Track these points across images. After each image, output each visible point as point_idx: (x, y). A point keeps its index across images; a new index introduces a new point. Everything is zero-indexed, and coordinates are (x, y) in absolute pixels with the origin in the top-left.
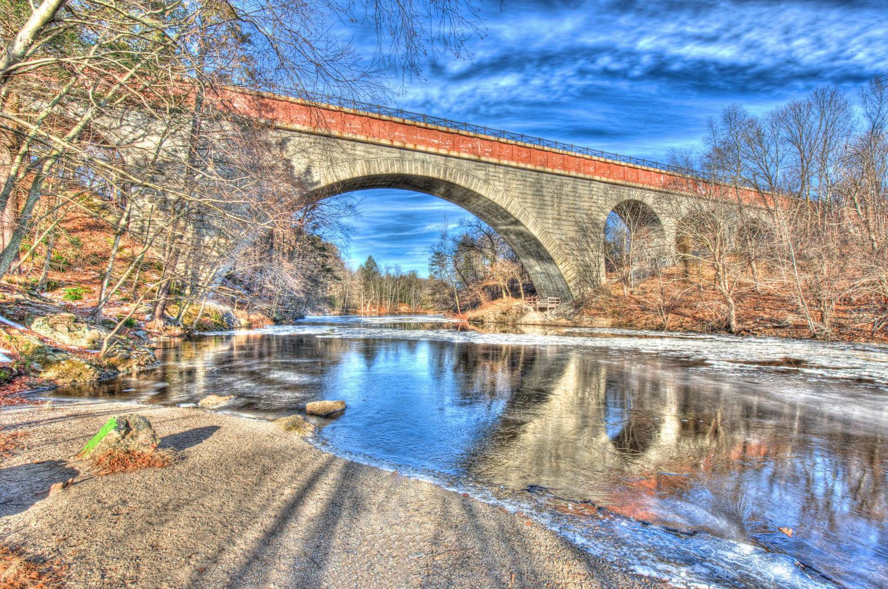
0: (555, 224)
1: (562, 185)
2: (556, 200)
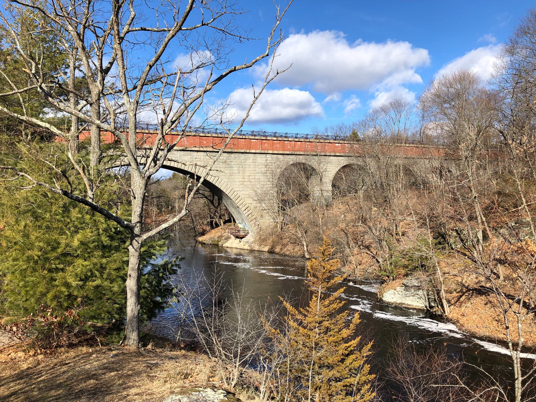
0: (241, 184)
1: (246, 160)
2: (240, 169)
